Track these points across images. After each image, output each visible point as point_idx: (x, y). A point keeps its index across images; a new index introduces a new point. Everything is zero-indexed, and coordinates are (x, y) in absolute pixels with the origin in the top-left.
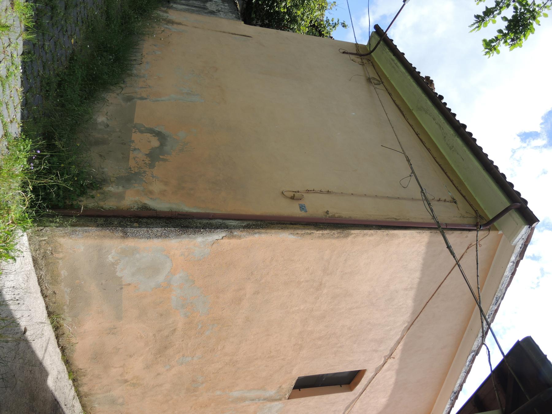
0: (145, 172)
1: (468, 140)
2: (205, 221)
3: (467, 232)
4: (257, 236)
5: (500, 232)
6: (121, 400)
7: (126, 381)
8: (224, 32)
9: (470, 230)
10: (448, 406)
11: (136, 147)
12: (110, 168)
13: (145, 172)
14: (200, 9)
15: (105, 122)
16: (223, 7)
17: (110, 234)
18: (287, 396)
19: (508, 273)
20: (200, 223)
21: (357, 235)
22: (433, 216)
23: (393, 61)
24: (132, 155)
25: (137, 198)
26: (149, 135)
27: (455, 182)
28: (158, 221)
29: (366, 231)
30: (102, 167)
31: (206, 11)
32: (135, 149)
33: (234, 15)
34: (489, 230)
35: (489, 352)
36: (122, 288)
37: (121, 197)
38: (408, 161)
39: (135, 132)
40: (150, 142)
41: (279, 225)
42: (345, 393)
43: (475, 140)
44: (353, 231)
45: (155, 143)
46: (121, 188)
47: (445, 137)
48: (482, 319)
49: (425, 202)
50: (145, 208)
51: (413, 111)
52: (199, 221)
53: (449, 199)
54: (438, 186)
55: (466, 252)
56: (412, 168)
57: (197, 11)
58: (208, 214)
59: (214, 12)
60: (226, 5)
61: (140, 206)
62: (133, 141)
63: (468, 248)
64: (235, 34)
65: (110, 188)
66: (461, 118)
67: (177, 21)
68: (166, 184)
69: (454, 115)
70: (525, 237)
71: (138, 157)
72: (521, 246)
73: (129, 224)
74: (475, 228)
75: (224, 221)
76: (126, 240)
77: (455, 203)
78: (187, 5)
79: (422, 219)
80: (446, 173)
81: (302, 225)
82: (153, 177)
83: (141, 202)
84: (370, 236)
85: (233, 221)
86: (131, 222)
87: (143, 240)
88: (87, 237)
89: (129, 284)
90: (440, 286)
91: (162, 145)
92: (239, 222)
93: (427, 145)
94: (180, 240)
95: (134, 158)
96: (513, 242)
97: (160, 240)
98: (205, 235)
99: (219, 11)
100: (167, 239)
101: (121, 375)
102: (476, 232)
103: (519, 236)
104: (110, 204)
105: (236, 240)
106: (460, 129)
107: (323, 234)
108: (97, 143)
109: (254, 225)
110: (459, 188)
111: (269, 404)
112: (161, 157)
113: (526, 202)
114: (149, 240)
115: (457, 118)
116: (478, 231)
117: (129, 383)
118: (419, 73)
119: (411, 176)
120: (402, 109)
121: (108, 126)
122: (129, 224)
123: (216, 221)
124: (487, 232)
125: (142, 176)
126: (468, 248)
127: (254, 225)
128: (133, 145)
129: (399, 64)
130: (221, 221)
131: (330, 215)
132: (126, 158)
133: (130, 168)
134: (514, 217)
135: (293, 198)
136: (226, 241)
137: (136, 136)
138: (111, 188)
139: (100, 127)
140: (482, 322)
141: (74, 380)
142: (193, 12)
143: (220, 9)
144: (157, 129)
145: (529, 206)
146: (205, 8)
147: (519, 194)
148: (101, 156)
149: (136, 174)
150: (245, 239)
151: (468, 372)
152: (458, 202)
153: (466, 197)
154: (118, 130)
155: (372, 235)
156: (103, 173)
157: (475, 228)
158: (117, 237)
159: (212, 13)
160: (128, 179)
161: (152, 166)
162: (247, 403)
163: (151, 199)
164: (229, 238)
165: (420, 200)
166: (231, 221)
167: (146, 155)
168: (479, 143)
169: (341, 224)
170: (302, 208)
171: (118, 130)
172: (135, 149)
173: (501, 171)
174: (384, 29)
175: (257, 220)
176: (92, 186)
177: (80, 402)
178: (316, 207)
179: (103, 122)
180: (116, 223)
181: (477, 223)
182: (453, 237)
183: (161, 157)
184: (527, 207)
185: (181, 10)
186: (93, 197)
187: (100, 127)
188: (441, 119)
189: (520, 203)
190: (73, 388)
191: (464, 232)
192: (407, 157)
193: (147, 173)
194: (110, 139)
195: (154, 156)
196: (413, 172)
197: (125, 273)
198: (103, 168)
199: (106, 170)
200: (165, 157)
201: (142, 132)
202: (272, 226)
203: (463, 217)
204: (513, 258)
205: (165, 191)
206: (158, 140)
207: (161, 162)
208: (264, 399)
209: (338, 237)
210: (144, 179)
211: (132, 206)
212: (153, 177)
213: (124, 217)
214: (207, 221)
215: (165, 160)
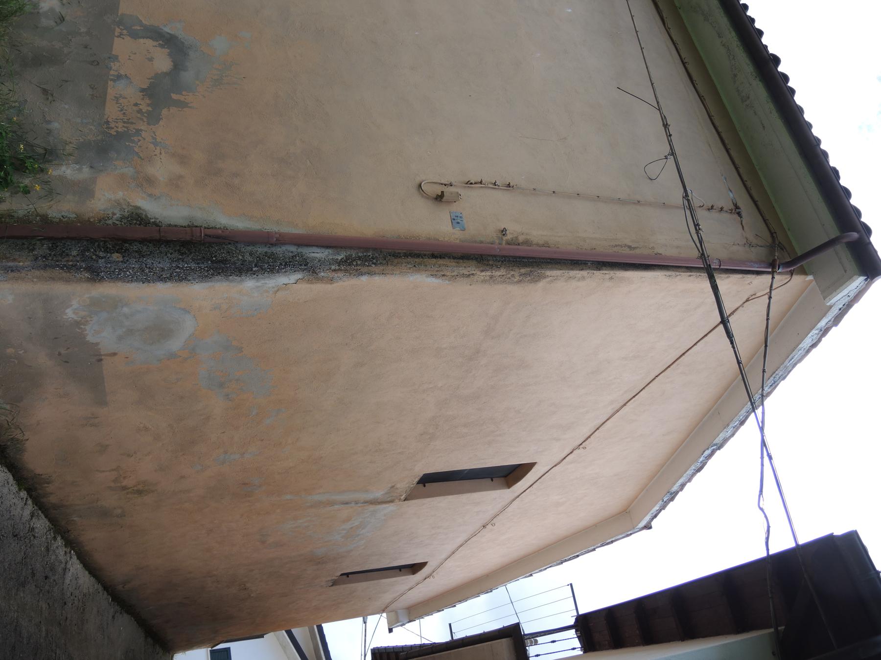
0: (138, 132)
1: (778, 90)
2: (261, 250)
3: (754, 276)
4: (364, 279)
5: (810, 278)
6: (119, 511)
7: (124, 488)
9: (758, 273)
10: (657, 508)
11: (122, 72)
12: (65, 123)
13: (138, 132)
15: (58, 9)
17: (64, 274)
18: (403, 497)
19: (807, 342)
20: (251, 254)
21: (556, 278)
22: (703, 254)
24: (111, 92)
25: (120, 195)
26: (149, 43)
27: (741, 170)
28: (163, 249)
29: (572, 273)
30: (48, 118)
32: (119, 77)
34: (792, 273)
35: (769, 527)
36: (101, 360)
37: (85, 190)
38: (666, 126)
39: (120, 35)
40: (151, 60)
41: (409, 259)
42: (498, 492)
43: (792, 91)
44: (548, 273)
45: (162, 62)
46: (86, 169)
47: (735, 76)
48: (762, 458)
49: (688, 212)
50: (138, 218)
52: (250, 248)
53: (729, 206)
54: (712, 181)
55: (742, 305)
56: (670, 142)
58: (269, 235)
61: (126, 214)
62: (116, 58)
63: (747, 300)
65: (64, 168)
66: (772, 42)
68: (183, 160)
69: (760, 33)
70: (852, 295)
71: (125, 94)
72: (841, 306)
73: (101, 254)
74: (770, 270)
75: (300, 250)
76: (98, 285)
77: (739, 214)
79: (678, 247)
80: (727, 151)
81: (454, 258)
82: (156, 144)
83: (129, 204)
84: (579, 280)
85: (318, 250)
86: (106, 250)
87: (134, 285)
88: (17, 279)
89: (115, 354)
90: (683, 354)
91: (178, 67)
92: (330, 251)
94: (210, 284)
95: (117, 99)
96: (830, 300)
97: (169, 285)
98: (260, 276)
100: (184, 283)
101: (115, 481)
102: (770, 276)
103: (845, 292)
104: (63, 208)
105: (323, 285)
106: (766, 65)
107: (491, 277)
108: (38, 60)
109: (360, 258)
110: (749, 184)
111: (372, 508)
112: (174, 96)
113: (868, 231)
114: (146, 284)
115: (765, 40)
116: (772, 273)
117: (130, 490)
119: (666, 158)
120: (726, 142)
121: (62, 19)
122: (101, 254)
123: (284, 248)
124: (788, 277)
125: (133, 141)
126: (747, 300)
127: (360, 258)
128: (115, 66)
130: (293, 249)
131: (509, 237)
132: (99, 98)
133: (107, 122)
134: (841, 252)
135: (439, 198)
136: (304, 287)
137: (122, 46)
138: (66, 171)
139: (45, 22)
140: (762, 458)
141: (29, 491)
144: (167, 29)
145: (873, 239)
147: (858, 213)
148: (45, 91)
149: (119, 136)
150: (341, 283)
151: (699, 470)
152: (744, 214)
153: (759, 203)
154: (83, 30)
155: (583, 278)
156: (49, 132)
157: (770, 270)
158: (80, 280)
160: (105, 147)
161: (153, 118)
162: (336, 507)
163: (150, 195)
164: (309, 282)
165: (677, 207)
166: (315, 249)
167: (143, 90)
168: (798, 99)
169: (528, 258)
170: (456, 221)
171: (83, 30)
172: (119, 77)
173: (832, 163)
175: (367, 249)
176: (20, 166)
177: (46, 517)
178: (486, 217)
179: (52, 10)
180: (74, 253)
181: (774, 261)
182: (725, 283)
183: (174, 96)
184: (870, 243)
186: (26, 191)
187: (45, 22)
188: (732, 37)
189: (858, 232)
190: (30, 502)
191: (749, 276)
192: (664, 118)
193: (143, 134)
194: (66, 50)
195: (160, 94)
196: (673, 153)
197: (102, 335)
198: (49, 122)
199: (55, 125)
200: (182, 98)
201: (134, 35)
202: (396, 261)
203: (751, 245)
204: (822, 323)
205: (180, 177)
206: (170, 55)
207: (173, 110)
208: (365, 502)
209: (519, 282)
210: (136, 149)
211: (110, 212)
212: (156, 144)
213: (92, 241)
214: (266, 249)
215: (182, 105)
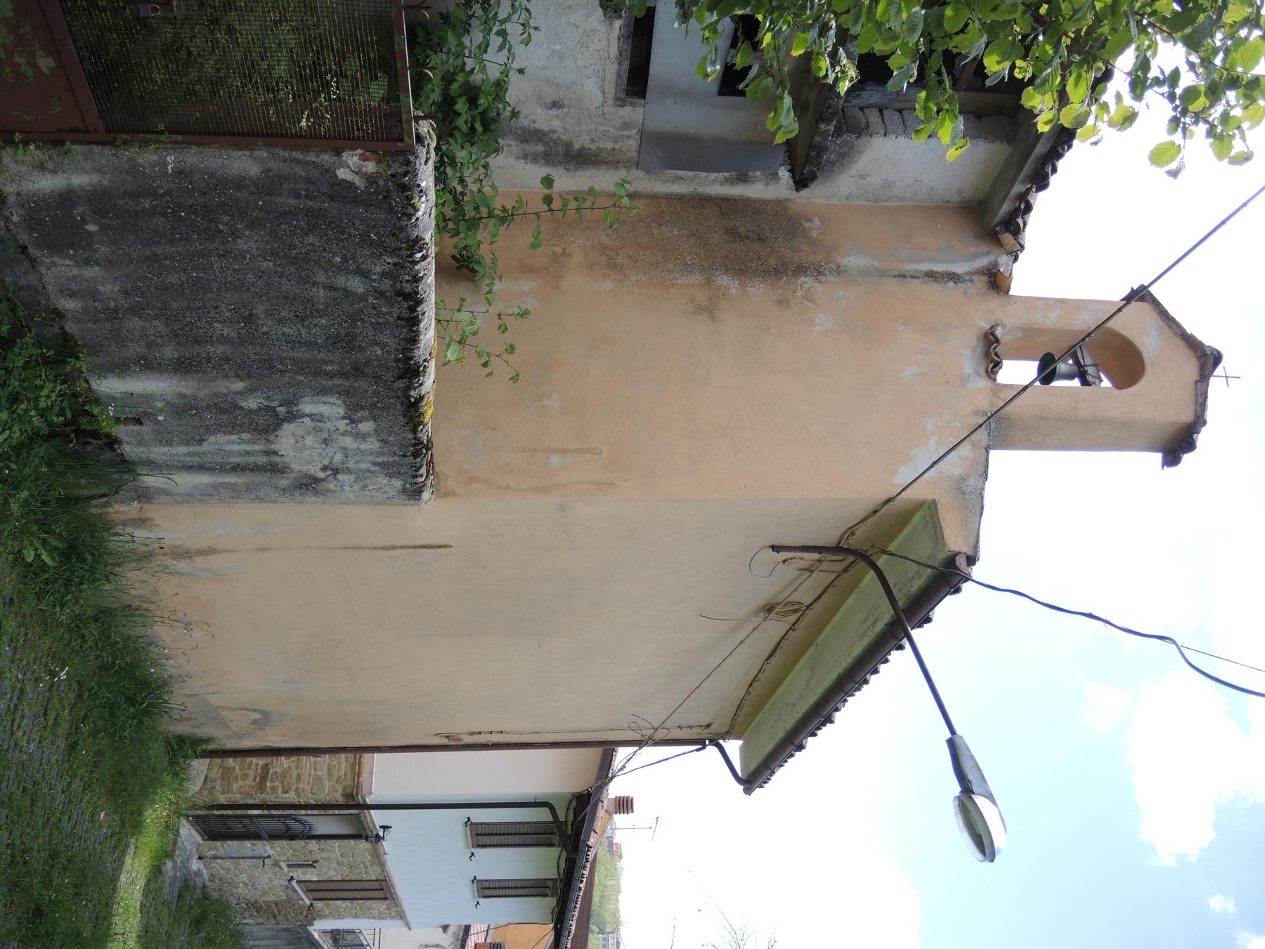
8: (356, 548)
14: (258, 478)
16: (348, 442)
23: (874, 623)
31: (283, 483)
33: (397, 483)
51: (813, 648)
57: (248, 488)
59: (316, 480)
60: (367, 426)
64: (394, 548)
67: (195, 544)
78: (201, 468)
93: (770, 668)
99: (336, 471)
106: (820, 713)
118: (887, 661)
129: (866, 642)
142: (236, 493)
143: (338, 458)
146: (275, 469)
159: (307, 484)
174: (976, 571)
182: (484, 935)
185: (189, 497)
